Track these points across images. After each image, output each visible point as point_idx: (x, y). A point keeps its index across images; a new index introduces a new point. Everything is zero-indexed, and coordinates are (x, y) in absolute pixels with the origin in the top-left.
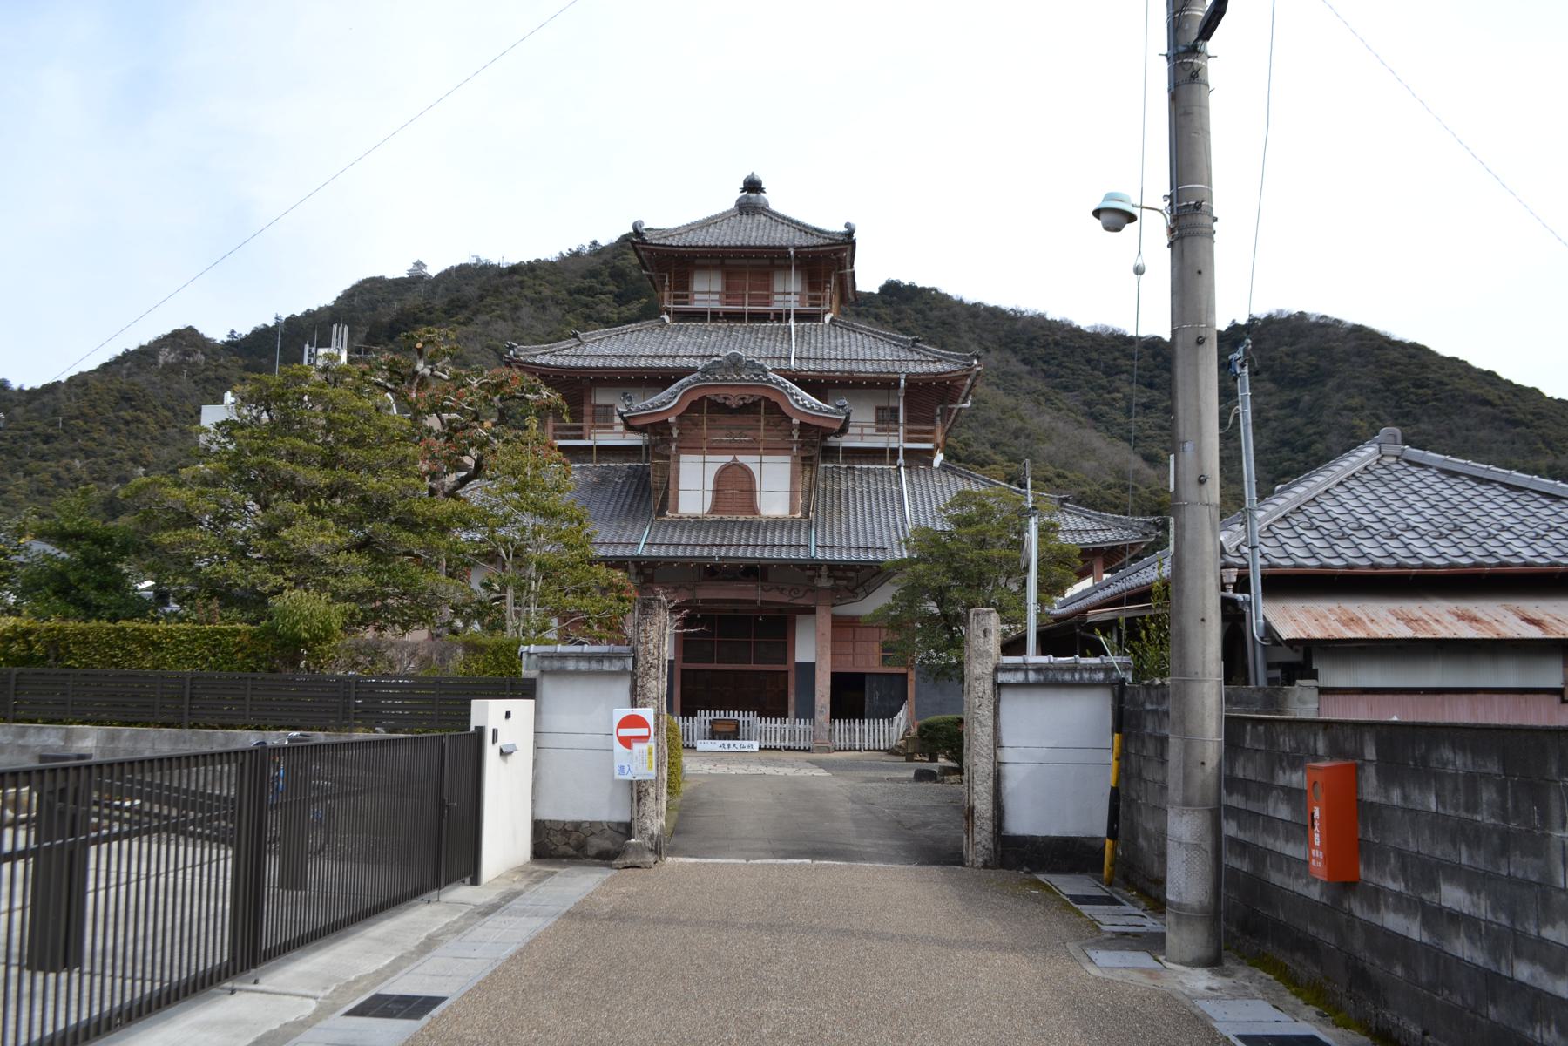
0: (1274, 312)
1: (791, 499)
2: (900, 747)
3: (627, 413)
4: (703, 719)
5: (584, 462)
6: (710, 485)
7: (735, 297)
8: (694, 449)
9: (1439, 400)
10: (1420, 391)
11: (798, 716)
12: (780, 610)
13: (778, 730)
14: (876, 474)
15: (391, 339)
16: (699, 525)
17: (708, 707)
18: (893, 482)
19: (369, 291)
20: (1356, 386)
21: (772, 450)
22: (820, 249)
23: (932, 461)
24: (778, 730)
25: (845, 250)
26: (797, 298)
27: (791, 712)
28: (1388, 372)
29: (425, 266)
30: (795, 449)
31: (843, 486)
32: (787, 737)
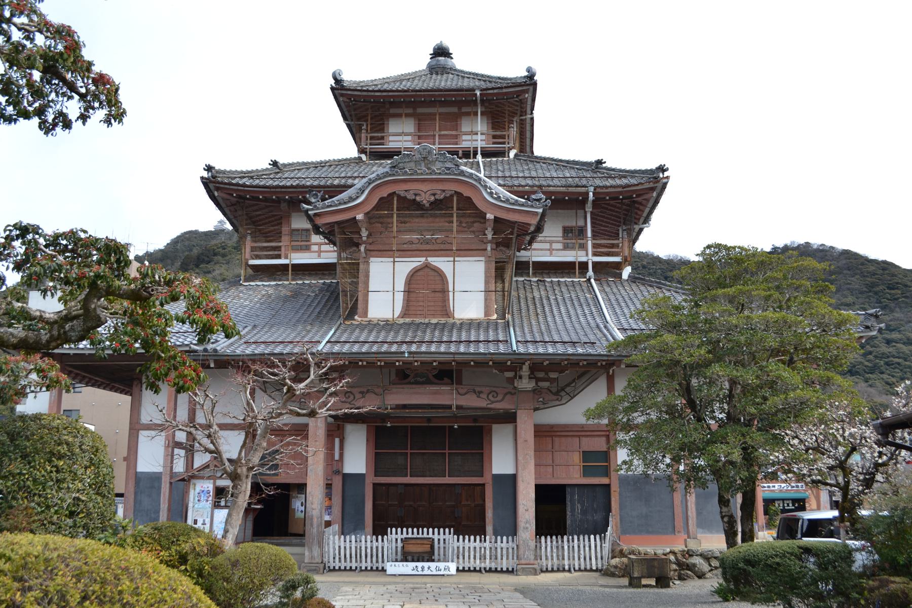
0: (789, 243)
1: (486, 300)
2: (616, 567)
3: (312, 210)
4: (395, 537)
5: (280, 280)
6: (401, 285)
7: (427, 137)
8: (384, 252)
9: (906, 297)
10: (893, 292)
11: (496, 534)
12: (475, 419)
13: (478, 549)
14: (566, 285)
15: (197, 266)
16: (389, 327)
17: (402, 524)
18: (585, 291)
19: (188, 239)
20: (849, 289)
21: (465, 251)
22: (504, 90)
23: (621, 274)
24: (478, 549)
25: (527, 91)
26: (484, 137)
27: (489, 529)
28: (869, 279)
29: (202, 178)
30: (489, 248)
31: (536, 294)
32: (488, 557)
